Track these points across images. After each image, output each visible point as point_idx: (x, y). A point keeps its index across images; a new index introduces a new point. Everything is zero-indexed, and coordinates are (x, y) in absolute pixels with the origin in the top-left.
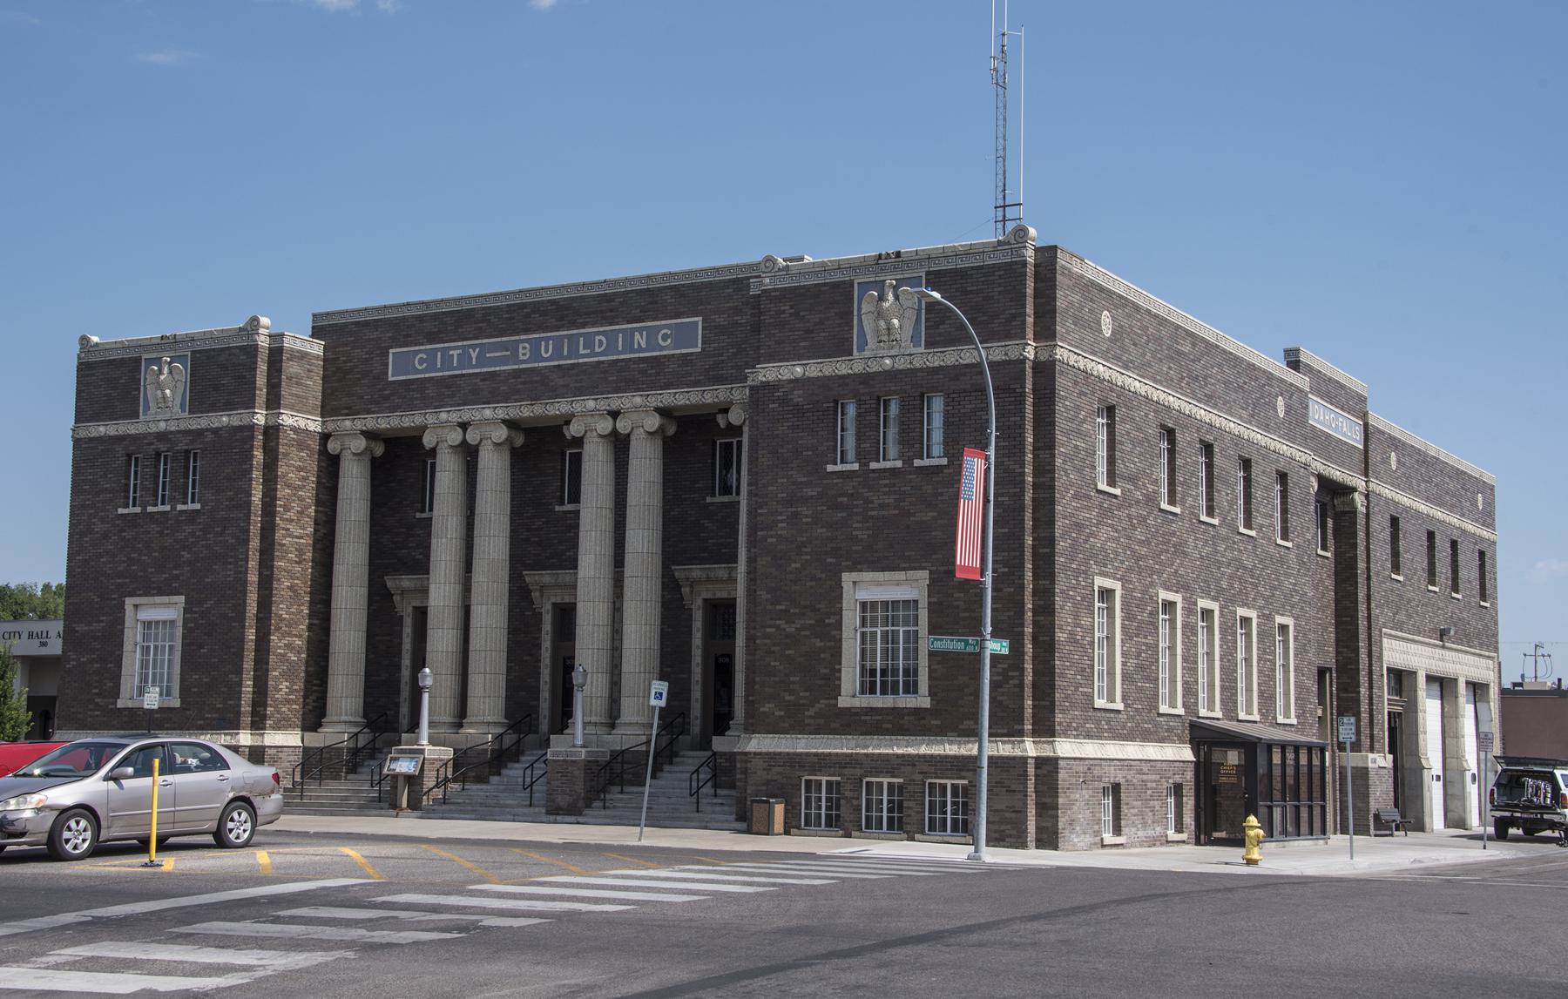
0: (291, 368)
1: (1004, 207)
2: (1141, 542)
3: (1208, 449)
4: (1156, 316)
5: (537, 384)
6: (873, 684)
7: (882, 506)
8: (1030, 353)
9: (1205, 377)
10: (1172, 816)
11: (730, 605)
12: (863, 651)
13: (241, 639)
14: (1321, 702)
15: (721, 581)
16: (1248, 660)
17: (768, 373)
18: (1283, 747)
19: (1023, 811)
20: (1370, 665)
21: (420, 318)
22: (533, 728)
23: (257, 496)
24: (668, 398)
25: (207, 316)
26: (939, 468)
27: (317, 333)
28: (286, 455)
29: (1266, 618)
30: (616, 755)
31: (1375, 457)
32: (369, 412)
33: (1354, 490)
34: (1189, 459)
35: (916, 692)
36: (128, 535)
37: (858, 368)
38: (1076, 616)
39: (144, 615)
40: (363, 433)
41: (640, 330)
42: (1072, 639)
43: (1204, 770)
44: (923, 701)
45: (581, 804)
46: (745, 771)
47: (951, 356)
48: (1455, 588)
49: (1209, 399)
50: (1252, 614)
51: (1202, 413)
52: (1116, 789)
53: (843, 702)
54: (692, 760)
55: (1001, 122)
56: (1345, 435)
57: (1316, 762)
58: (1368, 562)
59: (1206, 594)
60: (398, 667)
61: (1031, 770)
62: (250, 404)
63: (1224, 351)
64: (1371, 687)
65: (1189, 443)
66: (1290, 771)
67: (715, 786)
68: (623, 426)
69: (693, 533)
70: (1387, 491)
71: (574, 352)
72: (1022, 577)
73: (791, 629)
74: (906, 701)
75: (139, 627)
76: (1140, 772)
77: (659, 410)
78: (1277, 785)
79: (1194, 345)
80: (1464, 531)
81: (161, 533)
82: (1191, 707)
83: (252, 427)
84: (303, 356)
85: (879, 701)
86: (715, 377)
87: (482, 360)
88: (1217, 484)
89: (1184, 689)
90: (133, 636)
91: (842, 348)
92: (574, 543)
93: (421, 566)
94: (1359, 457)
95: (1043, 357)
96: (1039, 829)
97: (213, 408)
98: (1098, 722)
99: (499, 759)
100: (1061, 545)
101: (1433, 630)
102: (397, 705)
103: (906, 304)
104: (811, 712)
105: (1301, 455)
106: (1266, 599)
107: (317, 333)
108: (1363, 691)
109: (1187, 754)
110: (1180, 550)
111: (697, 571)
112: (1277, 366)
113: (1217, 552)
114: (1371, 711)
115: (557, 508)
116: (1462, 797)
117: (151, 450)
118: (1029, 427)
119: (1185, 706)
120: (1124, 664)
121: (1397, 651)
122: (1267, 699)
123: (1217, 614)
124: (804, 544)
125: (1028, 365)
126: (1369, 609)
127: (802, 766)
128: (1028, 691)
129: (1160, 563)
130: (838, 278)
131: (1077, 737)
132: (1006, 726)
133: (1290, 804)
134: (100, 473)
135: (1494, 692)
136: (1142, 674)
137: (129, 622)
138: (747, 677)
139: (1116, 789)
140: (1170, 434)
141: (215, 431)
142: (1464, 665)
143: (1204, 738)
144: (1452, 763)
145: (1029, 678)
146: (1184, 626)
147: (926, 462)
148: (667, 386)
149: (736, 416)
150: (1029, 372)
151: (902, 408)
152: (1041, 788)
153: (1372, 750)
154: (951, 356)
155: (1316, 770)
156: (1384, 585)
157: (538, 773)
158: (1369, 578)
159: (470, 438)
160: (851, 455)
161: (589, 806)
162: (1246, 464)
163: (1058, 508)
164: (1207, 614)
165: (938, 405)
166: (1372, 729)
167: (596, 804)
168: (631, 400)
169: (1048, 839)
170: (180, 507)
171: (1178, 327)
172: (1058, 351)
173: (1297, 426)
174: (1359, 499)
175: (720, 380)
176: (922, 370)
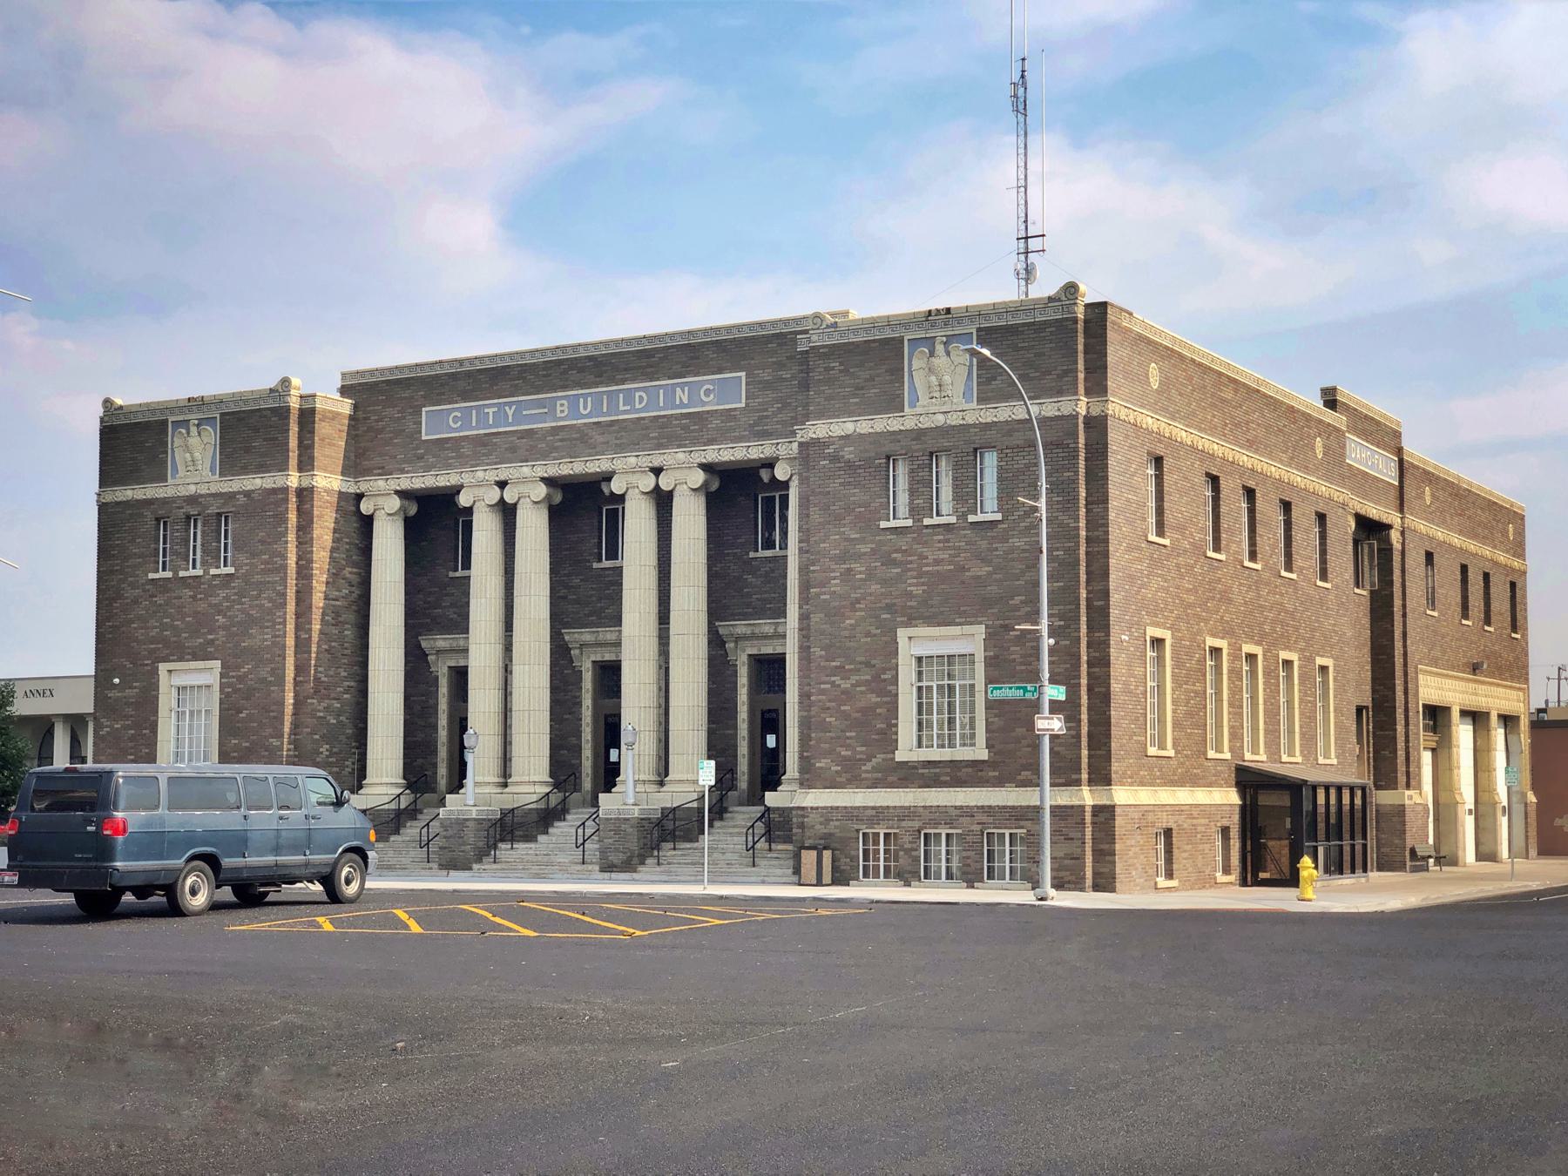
0: (322, 429)
1: (1027, 238)
2: (1189, 590)
3: (1250, 493)
4: (1200, 365)
6: (951, 737)
7: (937, 562)
9: (1247, 423)
10: (1162, 863)
11: (779, 661)
12: (920, 705)
13: (282, 703)
14: (1360, 741)
15: (766, 637)
16: (1290, 703)
17: (818, 429)
19: (1080, 858)
20: (1406, 703)
22: (577, 787)
25: (238, 374)
28: (321, 517)
29: (1308, 660)
30: (670, 813)
31: (1410, 493)
32: (402, 471)
33: (1390, 527)
34: (1235, 506)
35: (973, 745)
36: (159, 600)
37: (910, 424)
38: (1130, 666)
39: (179, 680)
40: (397, 492)
41: (682, 386)
43: (1249, 813)
44: (981, 753)
45: (635, 861)
46: (802, 826)
47: (1005, 412)
48: (1488, 621)
49: (1251, 444)
51: (1246, 458)
52: (1168, 833)
53: (900, 756)
54: (744, 815)
55: (1022, 151)
56: (1380, 472)
57: (1333, 801)
58: (1404, 599)
59: (1251, 639)
60: (435, 727)
61: (1088, 818)
62: (283, 467)
63: (1265, 395)
64: (1407, 724)
65: (1233, 490)
66: (1333, 809)
67: (770, 841)
69: (738, 587)
70: (1420, 525)
72: (1078, 630)
73: (846, 685)
74: (962, 753)
75: (174, 692)
76: (1191, 816)
77: (397, 492)
78: (1321, 826)
79: (1236, 391)
80: (1496, 563)
81: (194, 597)
82: (1236, 751)
83: (285, 490)
85: (935, 754)
86: (760, 433)
87: (518, 418)
88: (1260, 529)
89: (1230, 734)
90: (167, 700)
91: (894, 404)
92: (617, 599)
93: (460, 624)
94: (1394, 494)
95: (1095, 412)
96: (1096, 874)
97: (245, 470)
98: (1150, 769)
100: (1115, 598)
101: (1465, 664)
102: (435, 766)
103: (957, 360)
104: (869, 766)
106: (1307, 641)
107: (345, 391)
108: (1400, 728)
109: (1232, 797)
110: (1226, 598)
111: (741, 627)
112: (1312, 402)
113: (1259, 596)
114: (1407, 748)
115: (595, 565)
116: (1494, 831)
119: (1231, 750)
120: (1174, 711)
121: (1433, 687)
123: (1260, 658)
124: (858, 601)
125: (1081, 420)
126: (1405, 646)
127: (859, 820)
129: (1207, 610)
130: (888, 334)
131: (1131, 784)
132: (1066, 775)
138: (801, 733)
139: (1168, 833)
140: (1214, 480)
141: (248, 494)
142: (1496, 698)
143: (1249, 781)
144: (1484, 797)
146: (1230, 672)
148: (711, 442)
149: (781, 472)
150: (1081, 426)
152: (1098, 835)
153: (1408, 786)
154: (1005, 412)
156: (1424, 616)
157: (589, 832)
158: (1404, 615)
159: (511, 498)
161: (642, 863)
162: (1287, 506)
163: (1112, 561)
164: (1251, 658)
165: (991, 461)
166: (1408, 766)
167: (649, 861)
168: (672, 457)
169: (1104, 883)
170: (213, 571)
171: (1220, 374)
172: (1110, 406)
174: (1395, 536)
175: (765, 435)
176: (974, 425)
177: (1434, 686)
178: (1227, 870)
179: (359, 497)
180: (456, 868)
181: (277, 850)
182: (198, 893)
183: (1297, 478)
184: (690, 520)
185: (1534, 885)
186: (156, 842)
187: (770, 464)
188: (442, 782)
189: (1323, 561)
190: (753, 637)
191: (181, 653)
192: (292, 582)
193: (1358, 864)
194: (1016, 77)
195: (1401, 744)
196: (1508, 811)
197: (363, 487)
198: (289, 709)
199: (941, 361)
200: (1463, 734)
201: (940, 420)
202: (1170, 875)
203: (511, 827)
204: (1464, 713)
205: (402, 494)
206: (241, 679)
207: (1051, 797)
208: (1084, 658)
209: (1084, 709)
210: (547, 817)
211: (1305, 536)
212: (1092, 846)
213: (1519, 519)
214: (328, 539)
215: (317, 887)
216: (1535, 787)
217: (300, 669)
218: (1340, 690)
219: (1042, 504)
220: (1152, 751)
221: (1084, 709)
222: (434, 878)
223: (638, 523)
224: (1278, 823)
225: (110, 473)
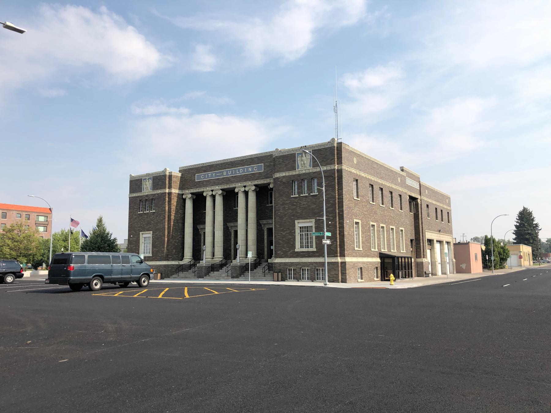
0: (174, 179)
5: (228, 180)
6: (308, 246)
7: (304, 205)
8: (336, 168)
10: (375, 274)
13: (164, 241)
17: (277, 175)
18: (401, 258)
19: (338, 275)
21: (202, 167)
23: (167, 209)
24: (256, 182)
26: (316, 195)
27: (180, 171)
29: (397, 228)
34: (377, 193)
37: (297, 173)
42: (349, 234)
43: (382, 263)
49: (381, 178)
50: (394, 227)
51: (380, 181)
52: (361, 268)
53: (296, 250)
59: (383, 223)
61: (340, 265)
62: (165, 188)
68: (247, 189)
69: (263, 212)
70: (425, 199)
71: (236, 173)
73: (284, 234)
74: (310, 249)
77: (255, 185)
78: (400, 266)
83: (165, 193)
84: (177, 177)
90: (142, 240)
91: (294, 169)
93: (204, 223)
96: (342, 278)
99: (221, 266)
100: (345, 212)
105: (405, 191)
108: (422, 244)
109: (378, 260)
110: (375, 213)
111: (265, 222)
116: (446, 268)
117: (144, 199)
118: (336, 185)
121: (429, 235)
122: (398, 247)
128: (338, 246)
130: (292, 152)
133: (404, 271)
134: (136, 204)
135: (452, 244)
136: (367, 242)
137: (141, 238)
139: (361, 268)
141: (158, 194)
142: (445, 238)
143: (383, 256)
144: (443, 260)
145: (338, 243)
147: (313, 194)
151: (308, 182)
154: (318, 169)
155: (410, 263)
156: (426, 219)
160: (296, 193)
164: (383, 227)
169: (344, 281)
173: (403, 184)
174: (419, 201)
177: (429, 235)
178: (377, 278)
179: (183, 194)
180: (200, 278)
181: (122, 274)
182: (97, 285)
183: (394, 186)
184: (252, 198)
185: (453, 280)
186: (83, 272)
187: (269, 184)
188: (233, 258)
189: (401, 206)
190: (268, 224)
191: (144, 230)
192: (167, 213)
193: (410, 275)
194: (335, 105)
195: (422, 248)
196: (449, 263)
197: (184, 192)
198: (166, 242)
199: (304, 158)
200: (437, 246)
201: (304, 171)
202: (362, 279)
203: (213, 268)
204: (437, 241)
205: (192, 194)
206: (156, 235)
207: (327, 260)
208: (338, 226)
209: (338, 239)
210: (221, 266)
211: (396, 200)
212: (339, 272)
213: (449, 198)
214: (175, 204)
215: (135, 283)
216: (455, 258)
217: (169, 233)
218: (406, 235)
219: (324, 189)
220: (356, 249)
221: (338, 239)
222: (195, 280)
223: (241, 199)
224: (390, 266)
225: (132, 190)
